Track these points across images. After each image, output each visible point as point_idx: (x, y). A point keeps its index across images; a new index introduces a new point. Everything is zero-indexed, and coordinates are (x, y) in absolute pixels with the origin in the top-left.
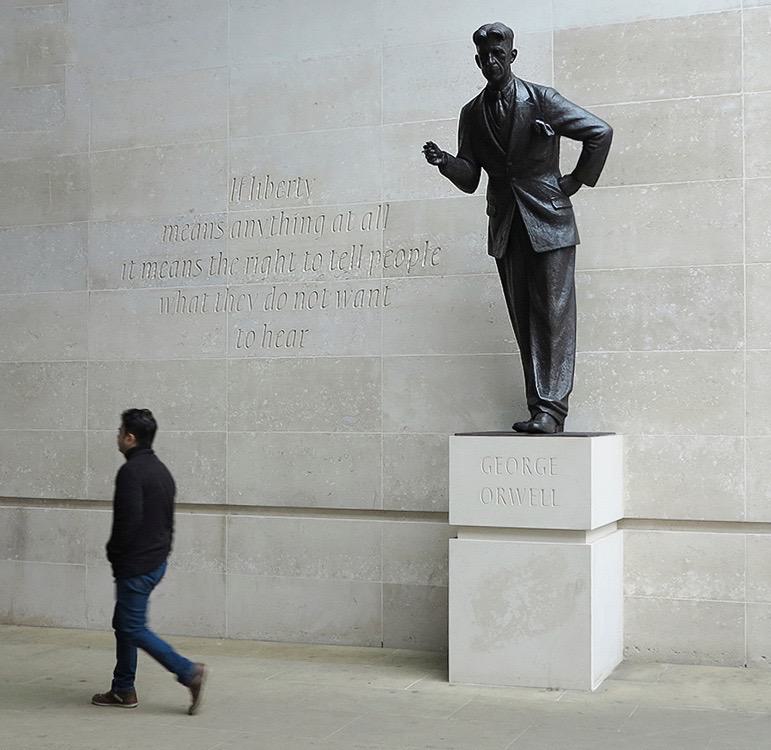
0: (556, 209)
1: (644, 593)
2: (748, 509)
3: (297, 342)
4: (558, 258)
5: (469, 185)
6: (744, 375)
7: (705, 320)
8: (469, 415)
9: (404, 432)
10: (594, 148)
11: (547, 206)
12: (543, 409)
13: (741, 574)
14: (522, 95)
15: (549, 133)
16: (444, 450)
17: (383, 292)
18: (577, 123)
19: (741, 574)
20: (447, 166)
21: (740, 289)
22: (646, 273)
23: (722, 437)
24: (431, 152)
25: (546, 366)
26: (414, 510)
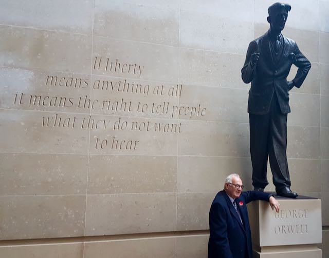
17: (178, 126)
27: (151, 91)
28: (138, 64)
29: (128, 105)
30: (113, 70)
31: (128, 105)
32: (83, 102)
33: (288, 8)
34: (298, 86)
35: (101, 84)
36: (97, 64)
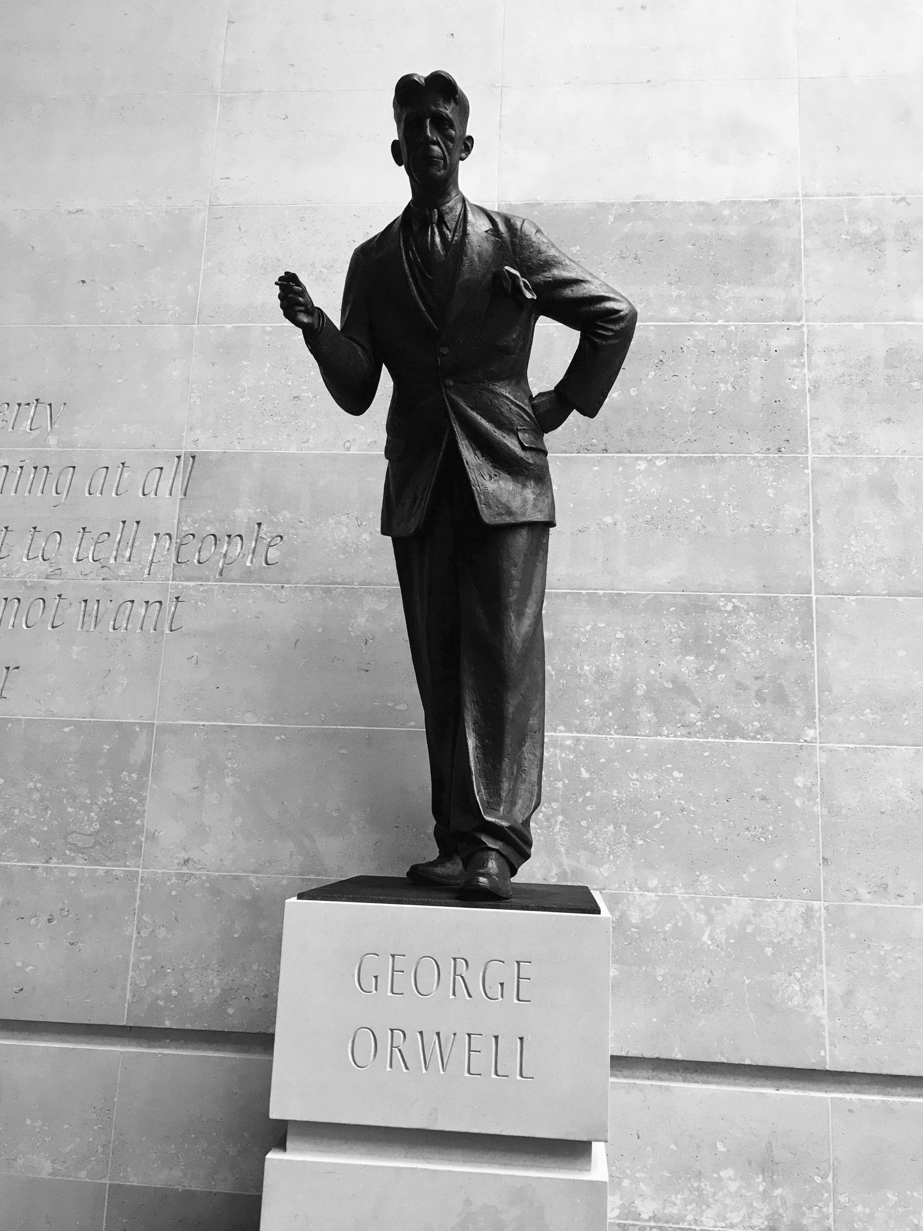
0: (524, 448)
1: (637, 1216)
2: (832, 1044)
4: (521, 540)
5: (353, 396)
6: (818, 789)
7: (745, 688)
8: (314, 841)
9: (185, 870)
11: (511, 443)
12: (490, 843)
13: (824, 1177)
14: (478, 227)
15: (529, 295)
16: (262, 943)
17: (169, 607)
18: (575, 288)
19: (824, 1177)
20: (316, 333)
21: (807, 636)
22: (643, 601)
23: (781, 902)
24: (292, 295)
25: (493, 750)
26: (188, 1026)
34: (590, 410)
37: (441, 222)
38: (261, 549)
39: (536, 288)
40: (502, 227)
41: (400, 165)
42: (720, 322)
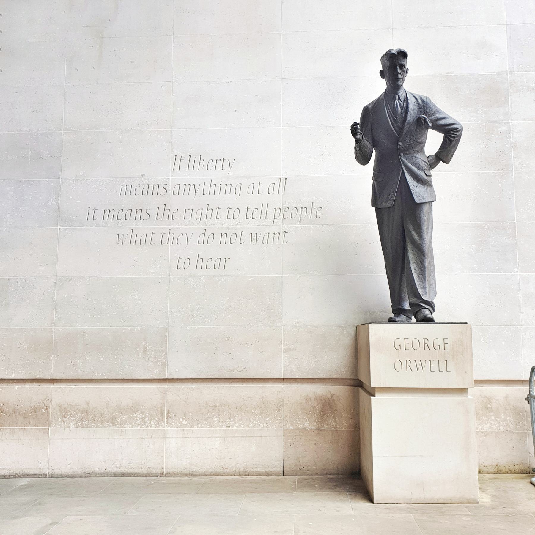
3: (222, 266)
4: (426, 208)
10: (454, 137)
17: (282, 234)
27: (244, 190)
28: (227, 158)
29: (215, 212)
30: (196, 169)
31: (215, 212)
32: (161, 211)
33: (403, 55)
34: (447, 162)
35: (182, 187)
36: (177, 164)
37: (399, 98)
38: (314, 212)
39: (432, 122)
40: (420, 101)
41: (383, 78)
42: (480, 122)
